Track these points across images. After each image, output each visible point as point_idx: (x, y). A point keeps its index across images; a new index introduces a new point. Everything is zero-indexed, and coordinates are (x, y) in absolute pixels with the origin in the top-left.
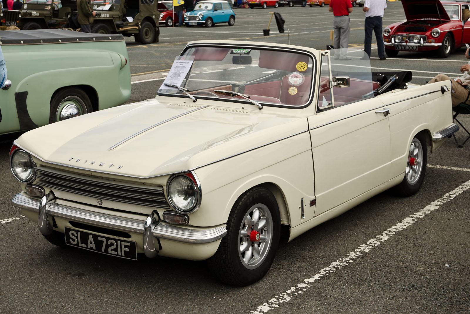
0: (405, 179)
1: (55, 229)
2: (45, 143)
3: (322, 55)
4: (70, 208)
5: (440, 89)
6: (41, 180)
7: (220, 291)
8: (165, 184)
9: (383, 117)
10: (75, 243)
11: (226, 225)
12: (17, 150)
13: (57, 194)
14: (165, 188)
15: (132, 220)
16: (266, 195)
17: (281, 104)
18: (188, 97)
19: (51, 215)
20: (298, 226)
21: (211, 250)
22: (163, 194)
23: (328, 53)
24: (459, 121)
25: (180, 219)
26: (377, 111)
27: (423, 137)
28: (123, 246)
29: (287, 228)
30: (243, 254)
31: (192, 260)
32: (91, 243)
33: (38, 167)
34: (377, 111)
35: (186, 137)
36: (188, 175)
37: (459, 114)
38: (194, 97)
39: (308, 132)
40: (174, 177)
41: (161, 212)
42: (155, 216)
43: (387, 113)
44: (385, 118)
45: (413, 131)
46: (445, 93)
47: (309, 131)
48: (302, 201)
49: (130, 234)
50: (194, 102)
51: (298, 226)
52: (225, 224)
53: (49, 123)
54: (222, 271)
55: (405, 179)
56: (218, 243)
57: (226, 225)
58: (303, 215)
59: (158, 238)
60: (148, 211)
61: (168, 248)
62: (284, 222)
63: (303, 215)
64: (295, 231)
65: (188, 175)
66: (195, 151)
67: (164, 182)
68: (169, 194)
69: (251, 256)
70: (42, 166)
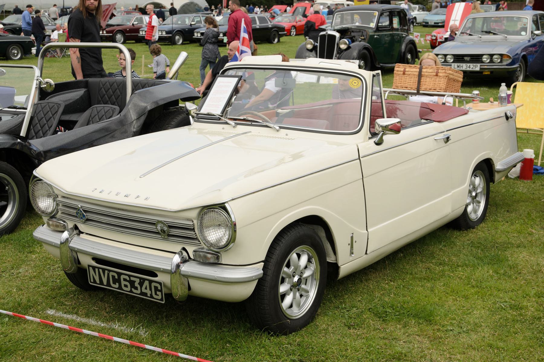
3: (374, 76)
4: (96, 243)
5: (504, 115)
7: (341, 302)
11: (263, 263)
13: (82, 227)
14: (195, 222)
15: (159, 257)
16: (309, 232)
17: (462, 92)
18: (227, 123)
19: (75, 251)
20: (347, 264)
26: (437, 137)
27: (485, 168)
29: (335, 267)
30: (283, 296)
31: (230, 301)
33: (60, 199)
34: (437, 137)
36: (222, 207)
39: (358, 160)
40: (206, 209)
41: (191, 250)
42: (185, 254)
43: (448, 139)
44: (445, 145)
47: (359, 159)
48: (352, 237)
49: (156, 272)
50: (234, 127)
51: (347, 264)
52: (262, 262)
53: (133, 136)
54: (258, 313)
56: (255, 284)
57: (263, 263)
58: (352, 253)
59: (187, 276)
60: (177, 248)
62: (331, 259)
63: (352, 253)
64: (345, 269)
67: (194, 214)
68: (201, 231)
69: (296, 303)
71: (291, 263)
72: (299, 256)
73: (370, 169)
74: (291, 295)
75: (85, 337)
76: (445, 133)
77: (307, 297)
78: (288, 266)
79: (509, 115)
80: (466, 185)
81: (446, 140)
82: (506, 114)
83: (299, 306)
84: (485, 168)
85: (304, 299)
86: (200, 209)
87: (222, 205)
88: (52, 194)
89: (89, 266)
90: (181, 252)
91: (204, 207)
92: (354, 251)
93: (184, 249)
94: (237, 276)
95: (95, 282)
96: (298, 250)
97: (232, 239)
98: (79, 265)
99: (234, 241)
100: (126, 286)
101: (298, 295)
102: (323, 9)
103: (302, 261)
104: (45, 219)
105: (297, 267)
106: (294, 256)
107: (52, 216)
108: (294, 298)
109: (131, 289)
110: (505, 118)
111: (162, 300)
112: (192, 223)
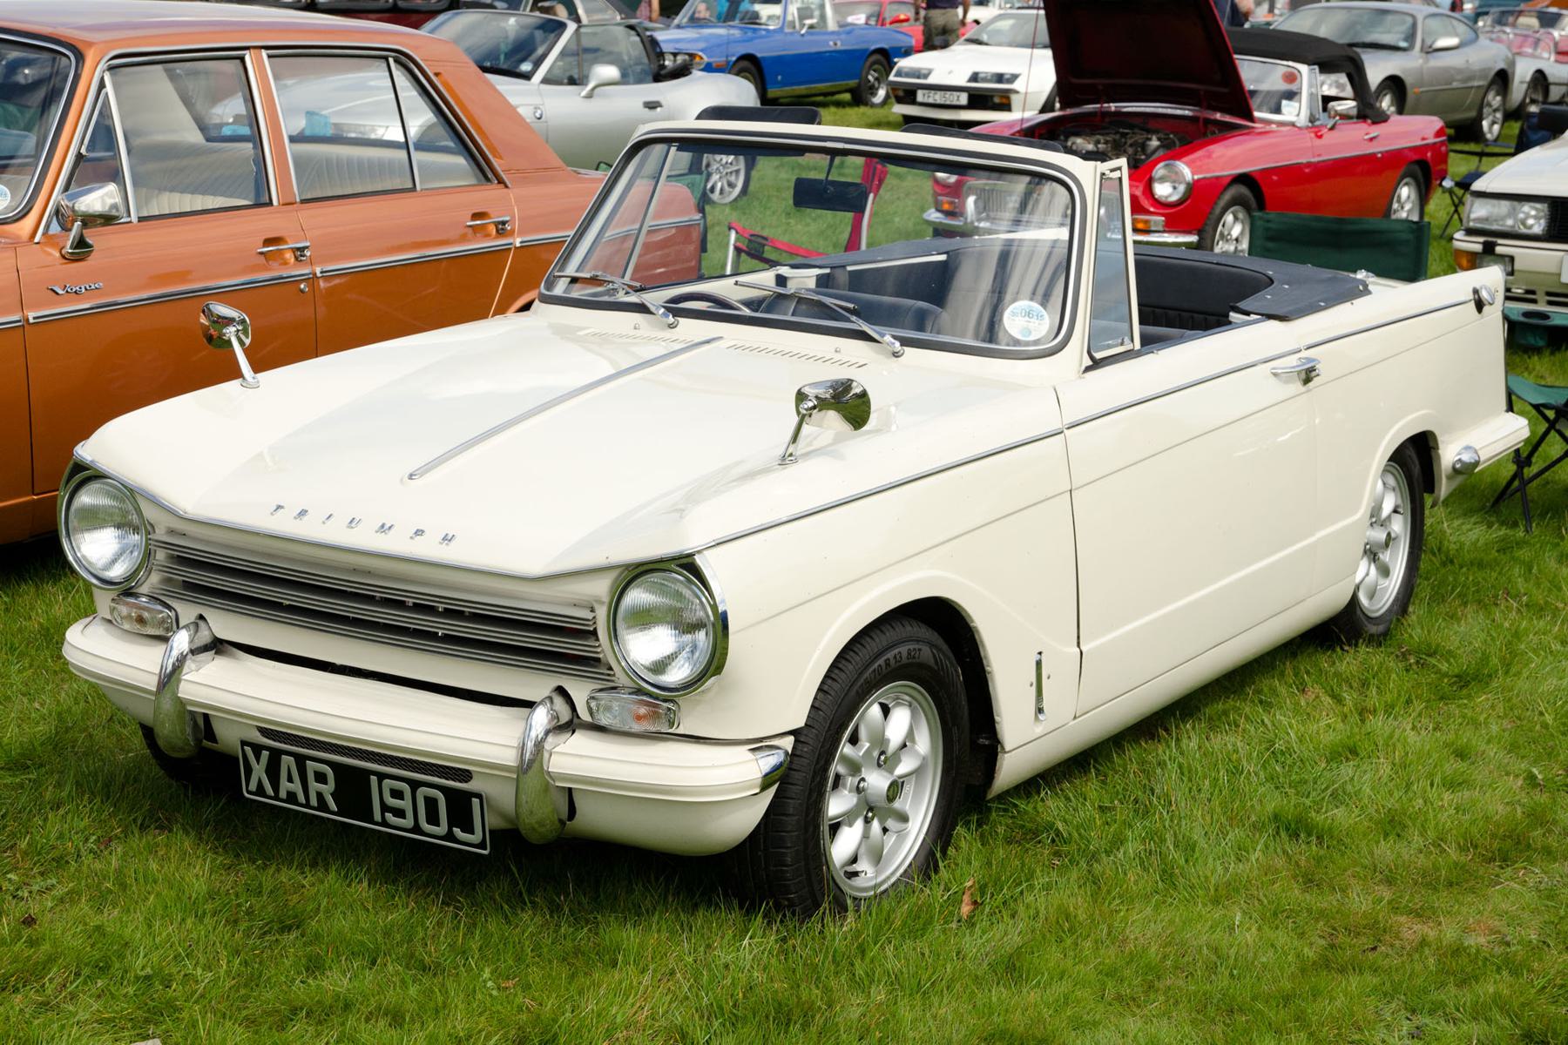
0: (1354, 601)
1: (206, 743)
2: (188, 456)
5: (1471, 296)
6: (168, 581)
8: (606, 599)
9: (1297, 386)
10: (408, 822)
12: (85, 475)
16: (929, 650)
21: (745, 820)
22: (594, 633)
23: (1120, 169)
24: (178, 211)
25: (659, 710)
28: (410, 814)
32: (290, 780)
35: (620, 479)
36: (687, 565)
37: (741, 158)
38: (895, 337)
41: (580, 692)
42: (559, 703)
44: (1303, 389)
45: (1385, 443)
46: (1486, 309)
54: (775, 869)
55: (1354, 601)
61: (595, 818)
63: (1040, 710)
65: (687, 565)
66: (695, 495)
67: (600, 588)
68: (614, 634)
70: (171, 532)
71: (863, 733)
72: (886, 710)
73: (1138, 489)
74: (859, 824)
75: (317, 937)
76: (1304, 354)
77: (902, 836)
78: (854, 740)
79: (1484, 295)
80: (1362, 511)
81: (1303, 376)
82: (1476, 291)
83: (878, 858)
84: (1415, 459)
85: (890, 840)
86: (613, 574)
87: (685, 561)
88: (129, 507)
89: (244, 743)
90: (550, 698)
91: (628, 567)
92: (1045, 705)
93: (561, 691)
94: (711, 780)
95: (260, 791)
96: (884, 693)
97: (715, 664)
98: (206, 743)
99: (719, 670)
100: (397, 794)
101: (876, 825)
102: (1443, 773)
103: (901, 726)
104: (103, 600)
105: (880, 741)
106: (875, 711)
107: (126, 590)
108: (866, 835)
109: (450, 830)
110: (1472, 304)
111: (482, 845)
112: (590, 616)
